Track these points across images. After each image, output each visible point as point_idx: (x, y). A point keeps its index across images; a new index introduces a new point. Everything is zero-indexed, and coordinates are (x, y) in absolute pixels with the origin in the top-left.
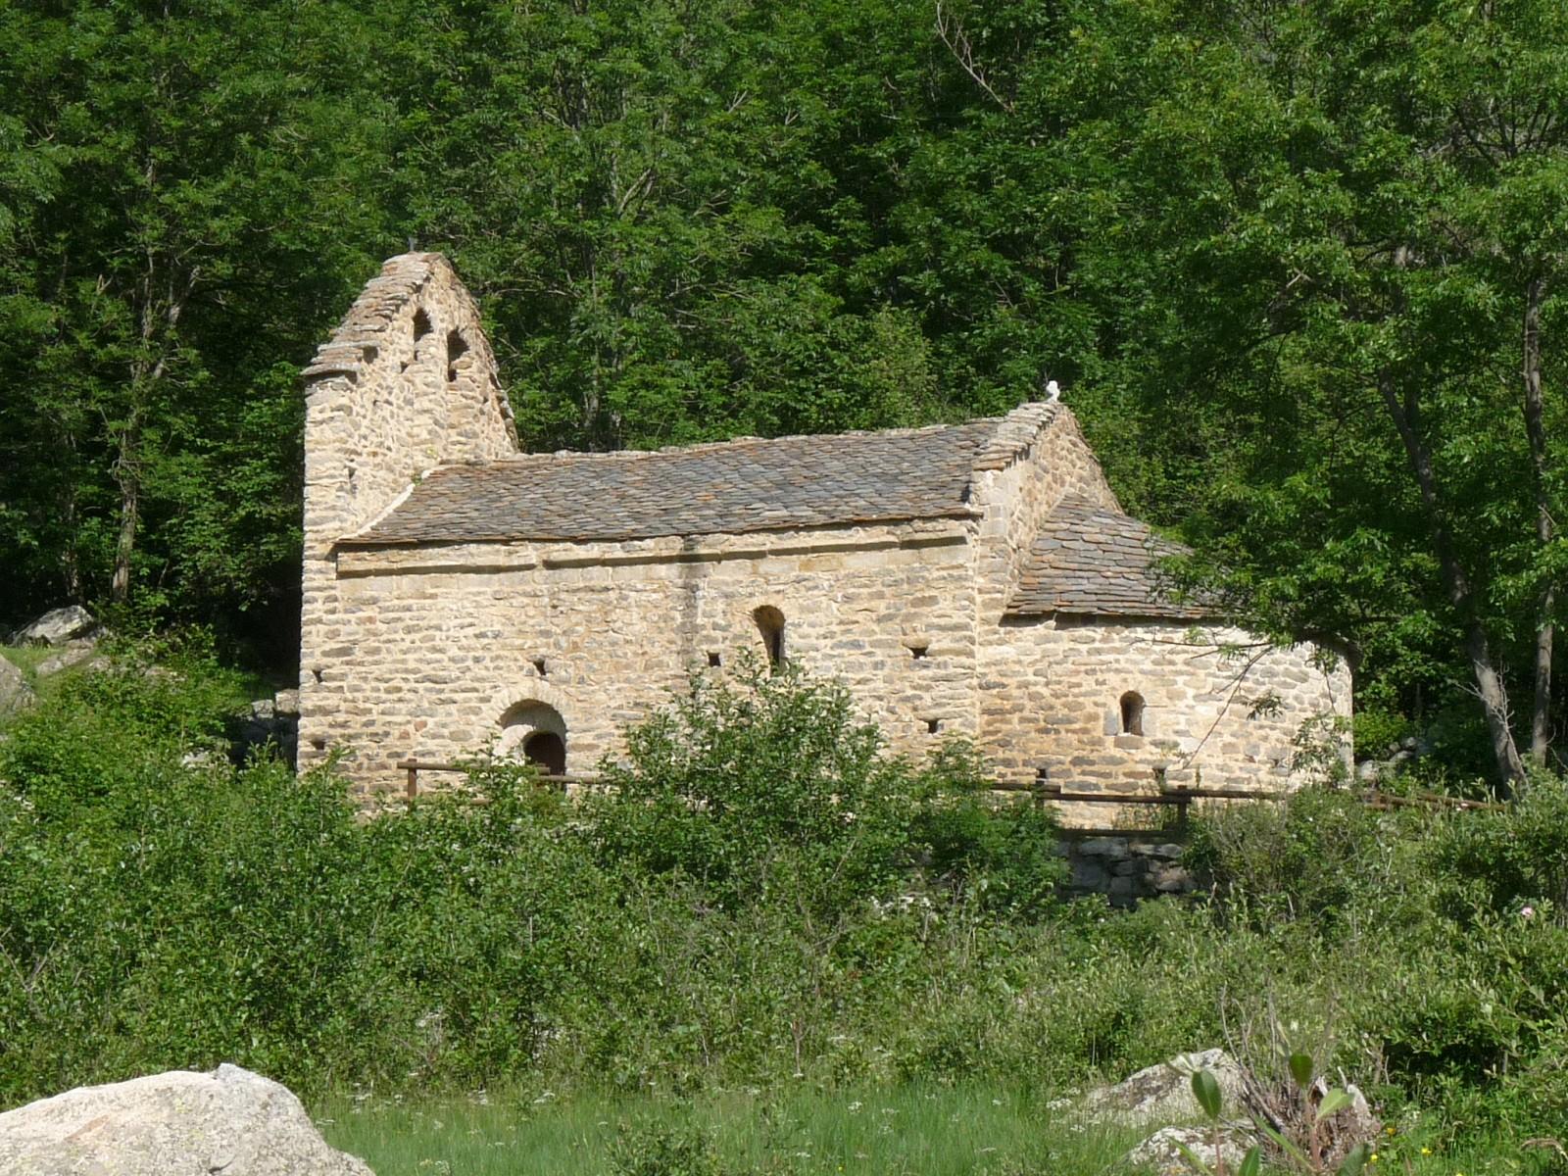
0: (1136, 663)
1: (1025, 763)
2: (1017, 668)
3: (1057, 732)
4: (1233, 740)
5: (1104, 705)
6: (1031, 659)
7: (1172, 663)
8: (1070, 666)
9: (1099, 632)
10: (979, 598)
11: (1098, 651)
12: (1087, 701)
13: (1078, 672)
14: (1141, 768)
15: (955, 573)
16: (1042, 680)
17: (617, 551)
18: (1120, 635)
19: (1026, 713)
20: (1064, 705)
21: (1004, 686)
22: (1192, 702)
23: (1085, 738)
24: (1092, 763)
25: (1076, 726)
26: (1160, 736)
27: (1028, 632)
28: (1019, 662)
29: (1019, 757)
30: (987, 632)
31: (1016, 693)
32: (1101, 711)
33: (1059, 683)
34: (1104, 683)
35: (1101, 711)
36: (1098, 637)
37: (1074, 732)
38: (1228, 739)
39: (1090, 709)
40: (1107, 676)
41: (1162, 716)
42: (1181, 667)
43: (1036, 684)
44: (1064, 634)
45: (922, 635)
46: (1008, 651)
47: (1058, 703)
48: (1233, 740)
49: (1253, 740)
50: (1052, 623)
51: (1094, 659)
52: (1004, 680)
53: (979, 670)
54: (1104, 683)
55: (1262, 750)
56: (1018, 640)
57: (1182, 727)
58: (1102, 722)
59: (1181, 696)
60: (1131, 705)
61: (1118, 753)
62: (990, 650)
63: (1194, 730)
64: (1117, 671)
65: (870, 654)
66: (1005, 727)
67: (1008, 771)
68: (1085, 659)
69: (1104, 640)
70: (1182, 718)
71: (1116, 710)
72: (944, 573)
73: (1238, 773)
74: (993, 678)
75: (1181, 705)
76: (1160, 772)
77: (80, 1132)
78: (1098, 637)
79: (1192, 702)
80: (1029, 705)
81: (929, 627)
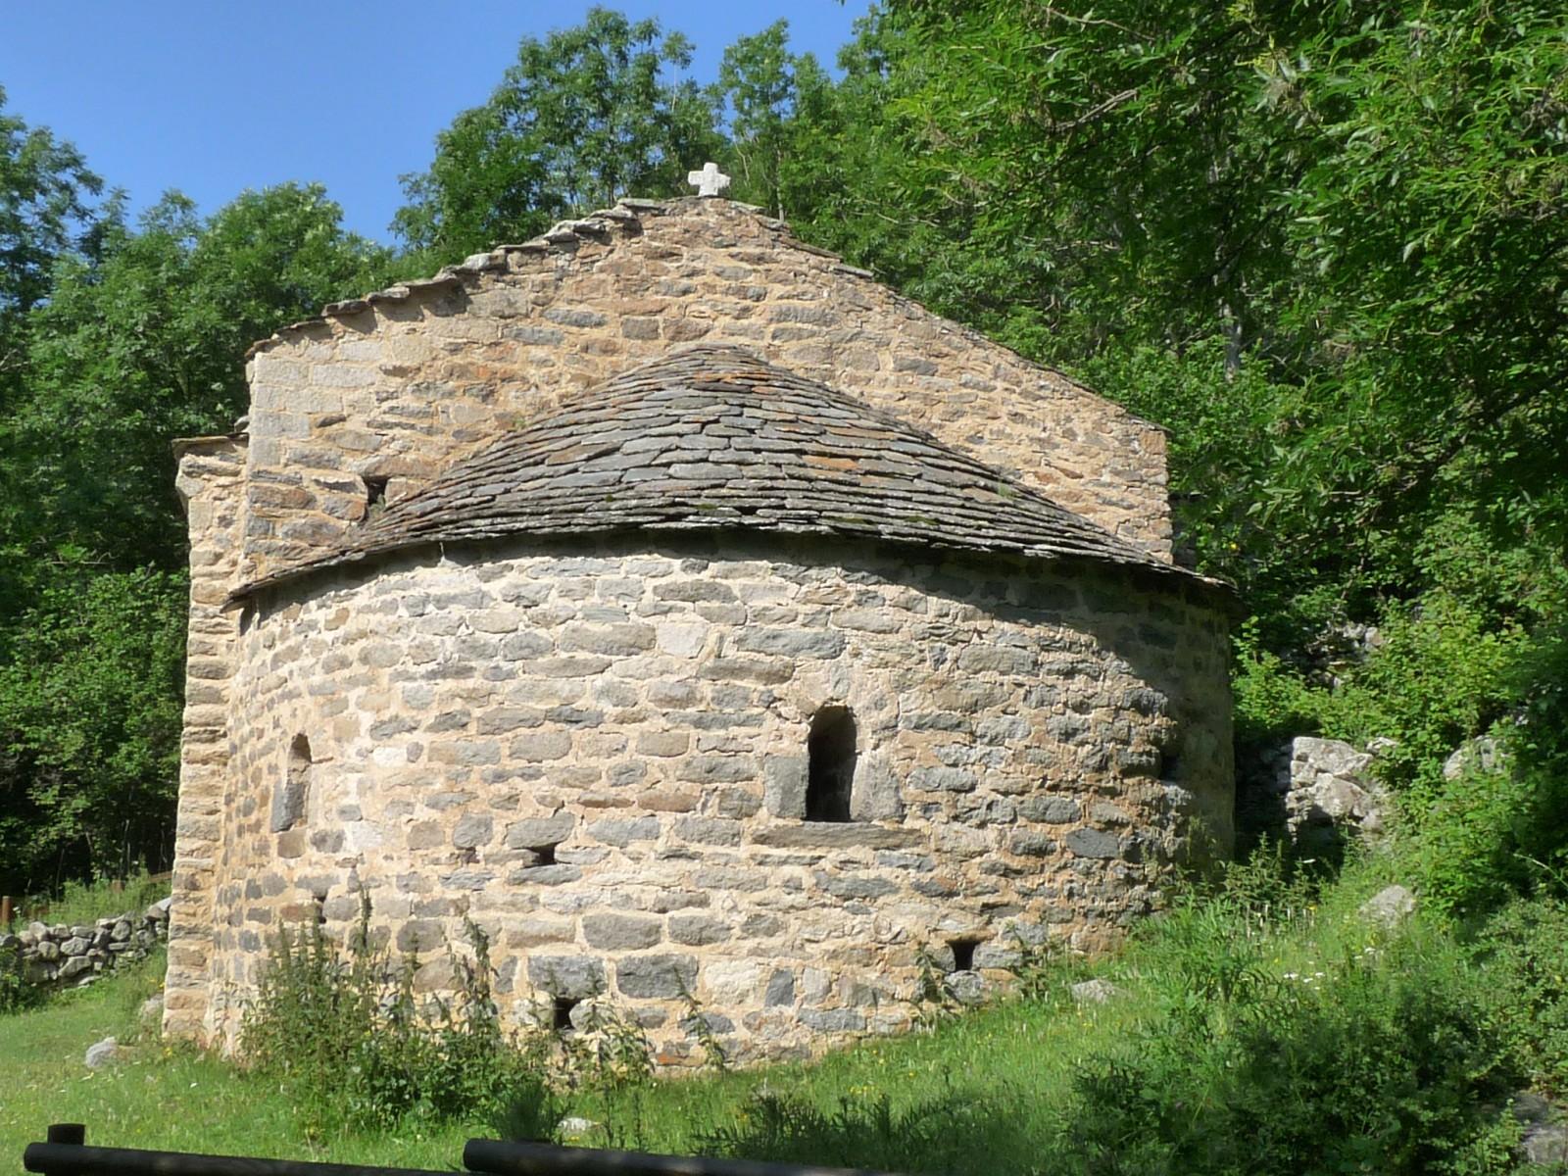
55: (498, 829)
73: (438, 891)
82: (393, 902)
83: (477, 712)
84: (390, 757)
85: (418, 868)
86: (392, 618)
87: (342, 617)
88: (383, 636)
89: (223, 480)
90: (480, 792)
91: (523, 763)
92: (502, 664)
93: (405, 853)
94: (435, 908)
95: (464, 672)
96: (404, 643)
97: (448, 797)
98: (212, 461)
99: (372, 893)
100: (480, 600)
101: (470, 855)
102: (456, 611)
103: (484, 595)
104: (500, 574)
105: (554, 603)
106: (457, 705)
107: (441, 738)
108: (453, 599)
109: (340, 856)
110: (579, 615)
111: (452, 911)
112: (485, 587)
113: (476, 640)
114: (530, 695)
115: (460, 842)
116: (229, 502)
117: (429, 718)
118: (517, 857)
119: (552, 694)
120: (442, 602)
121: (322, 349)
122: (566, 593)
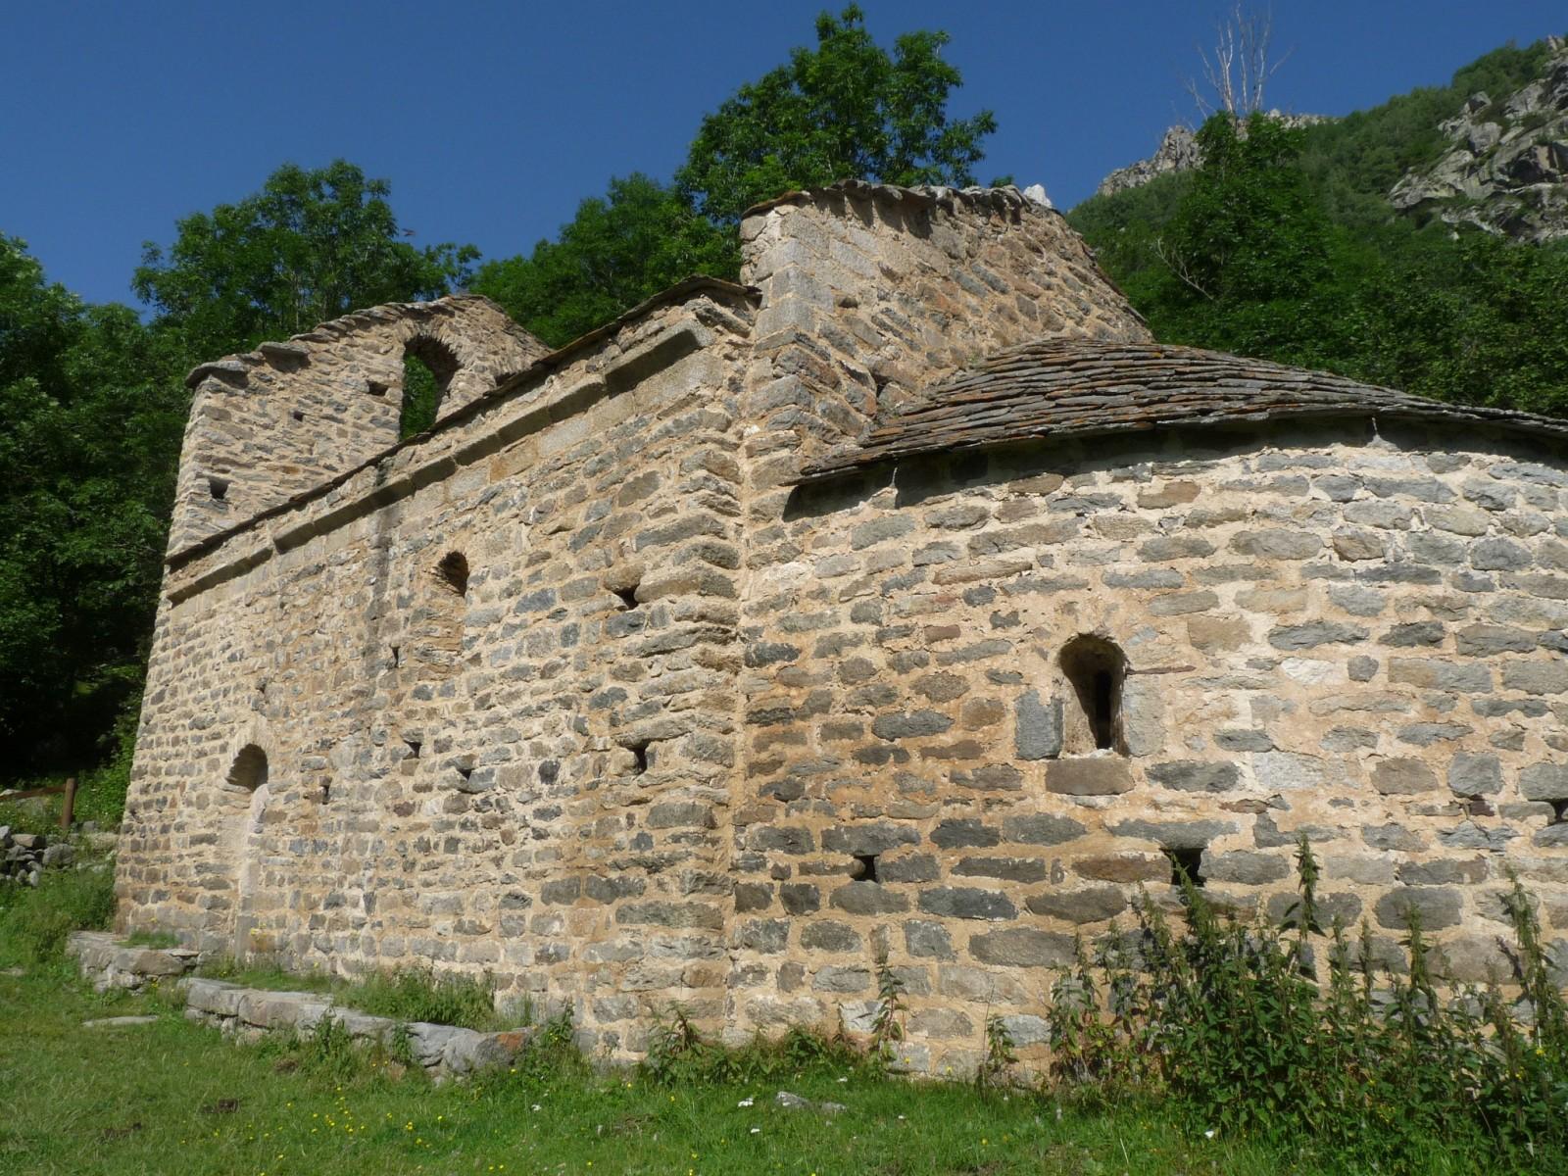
0: (1094, 559)
1: (830, 841)
2: (817, 607)
3: (902, 756)
4: (1411, 751)
5: (1017, 677)
6: (843, 583)
7: (1198, 549)
8: (928, 587)
9: (993, 498)
10: (746, 467)
11: (996, 543)
12: (971, 672)
13: (948, 601)
14: (1127, 847)
15: (683, 416)
16: (869, 629)
17: (320, 509)
18: (1045, 500)
19: (836, 716)
20: (919, 688)
21: (792, 653)
22: (1268, 652)
23: (968, 769)
24: (990, 838)
25: (947, 739)
26: (1176, 753)
27: (840, 523)
28: (821, 594)
29: (814, 823)
30: (760, 538)
31: (815, 667)
32: (1008, 695)
33: (906, 632)
34: (1013, 619)
35: (1008, 695)
36: (994, 506)
37: (942, 754)
38: (1391, 748)
39: (981, 691)
40: (1020, 602)
41: (1178, 694)
42: (1223, 558)
43: (857, 641)
44: (917, 513)
45: (632, 560)
46: (800, 572)
47: (902, 683)
48: (1411, 751)
49: (1477, 746)
50: (891, 492)
51: (987, 562)
52: (794, 641)
53: (744, 622)
54: (1013, 619)
55: (1509, 774)
56: (820, 543)
57: (1244, 723)
58: (1010, 724)
59: (1235, 635)
60: (1095, 672)
61: (1059, 807)
62: (767, 574)
63: (1280, 730)
64: (1047, 586)
65: (559, 614)
66: (792, 752)
67: (792, 861)
68: (966, 566)
69: (1008, 513)
70: (1242, 699)
71: (1049, 684)
72: (668, 422)
73: (1437, 850)
74: (771, 638)
75: (1236, 661)
76: (1186, 860)
77: (1165, 614)
78: (994, 506)
79: (1268, 652)
80: (841, 692)
81: (644, 538)
82: (1360, 862)
83: (1453, 627)
84: (1314, 674)
85: (1399, 816)
86: (1299, 500)
87: (1191, 492)
88: (1284, 520)
89: (735, 338)
90: (1474, 725)
91: (1522, 695)
92: (1472, 572)
93: (1375, 797)
94: (1436, 871)
95: (1425, 577)
96: (1325, 533)
97: (1432, 729)
98: (727, 312)
99: (1313, 847)
100: (1435, 493)
101: (1477, 805)
102: (1403, 502)
103: (1441, 487)
104: (1454, 467)
105: (1520, 509)
106: (1423, 615)
107: (1408, 654)
108: (1397, 487)
109: (1233, 796)
110: (1552, 528)
111: (1467, 877)
112: (1440, 478)
113: (1435, 539)
114: (1515, 614)
115: (1462, 787)
116: (740, 363)
117: (1384, 626)
118: (1540, 811)
119: (1538, 615)
120: (1381, 488)
121: (835, 223)
122: (1533, 500)
